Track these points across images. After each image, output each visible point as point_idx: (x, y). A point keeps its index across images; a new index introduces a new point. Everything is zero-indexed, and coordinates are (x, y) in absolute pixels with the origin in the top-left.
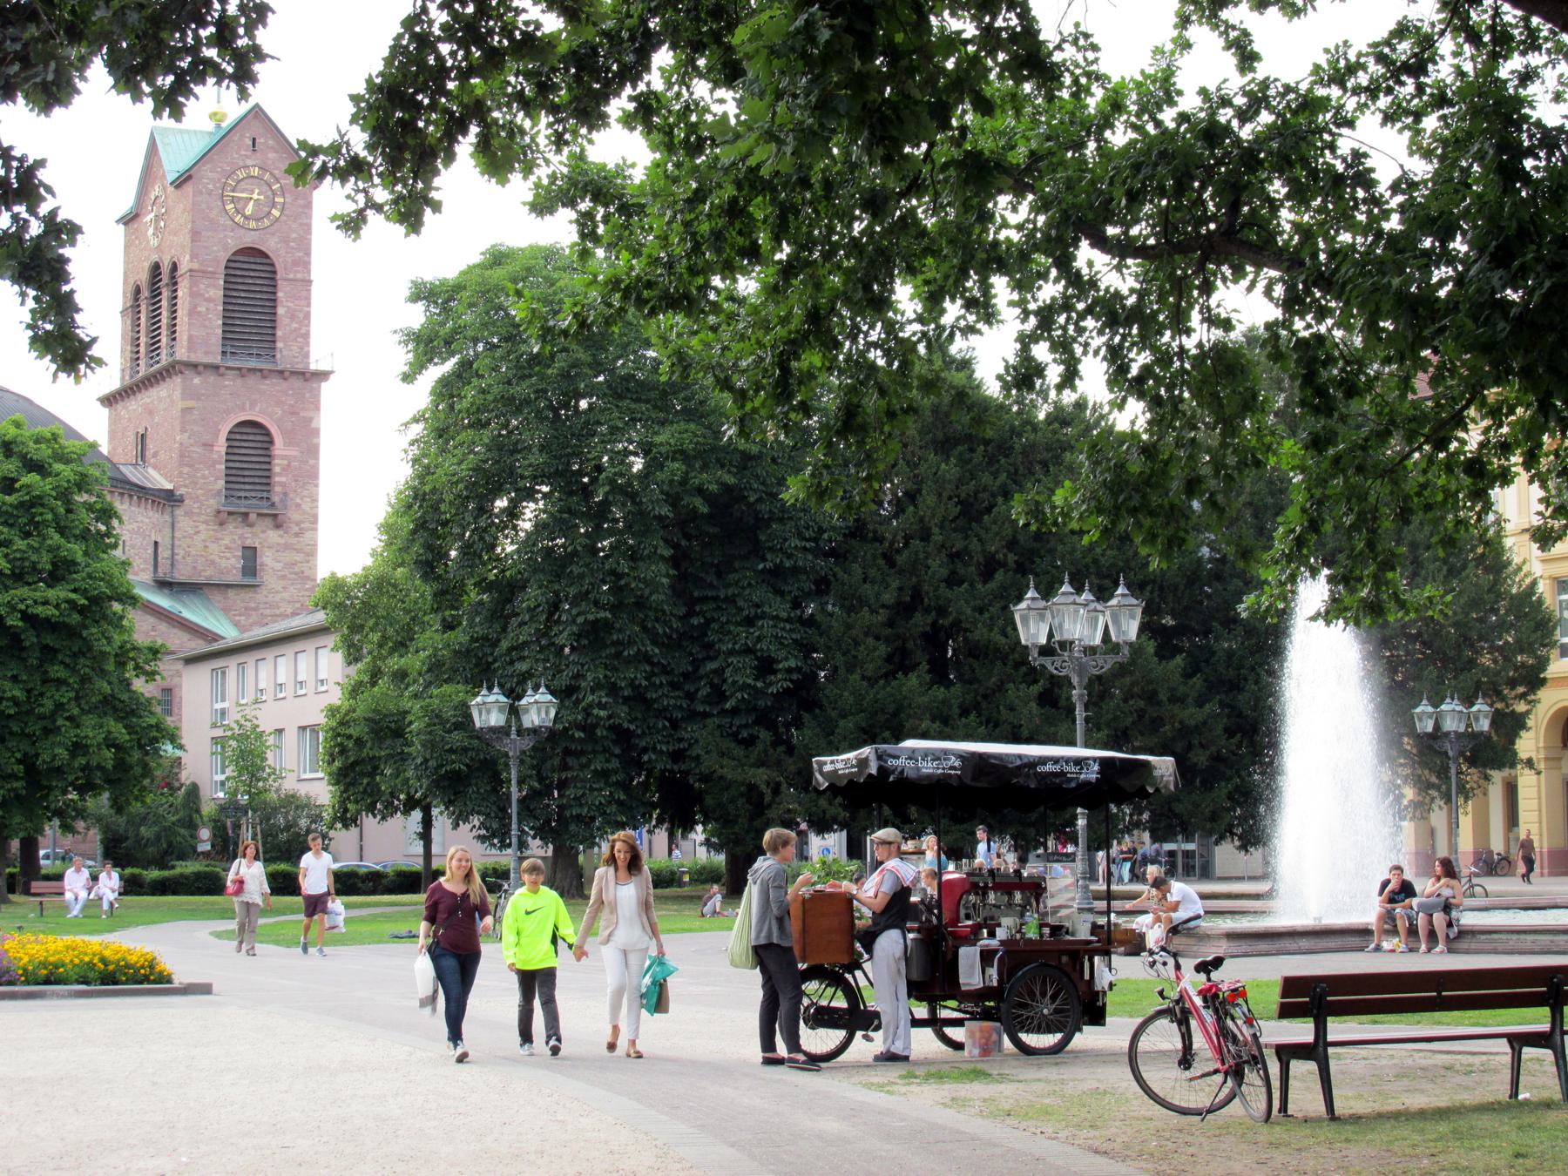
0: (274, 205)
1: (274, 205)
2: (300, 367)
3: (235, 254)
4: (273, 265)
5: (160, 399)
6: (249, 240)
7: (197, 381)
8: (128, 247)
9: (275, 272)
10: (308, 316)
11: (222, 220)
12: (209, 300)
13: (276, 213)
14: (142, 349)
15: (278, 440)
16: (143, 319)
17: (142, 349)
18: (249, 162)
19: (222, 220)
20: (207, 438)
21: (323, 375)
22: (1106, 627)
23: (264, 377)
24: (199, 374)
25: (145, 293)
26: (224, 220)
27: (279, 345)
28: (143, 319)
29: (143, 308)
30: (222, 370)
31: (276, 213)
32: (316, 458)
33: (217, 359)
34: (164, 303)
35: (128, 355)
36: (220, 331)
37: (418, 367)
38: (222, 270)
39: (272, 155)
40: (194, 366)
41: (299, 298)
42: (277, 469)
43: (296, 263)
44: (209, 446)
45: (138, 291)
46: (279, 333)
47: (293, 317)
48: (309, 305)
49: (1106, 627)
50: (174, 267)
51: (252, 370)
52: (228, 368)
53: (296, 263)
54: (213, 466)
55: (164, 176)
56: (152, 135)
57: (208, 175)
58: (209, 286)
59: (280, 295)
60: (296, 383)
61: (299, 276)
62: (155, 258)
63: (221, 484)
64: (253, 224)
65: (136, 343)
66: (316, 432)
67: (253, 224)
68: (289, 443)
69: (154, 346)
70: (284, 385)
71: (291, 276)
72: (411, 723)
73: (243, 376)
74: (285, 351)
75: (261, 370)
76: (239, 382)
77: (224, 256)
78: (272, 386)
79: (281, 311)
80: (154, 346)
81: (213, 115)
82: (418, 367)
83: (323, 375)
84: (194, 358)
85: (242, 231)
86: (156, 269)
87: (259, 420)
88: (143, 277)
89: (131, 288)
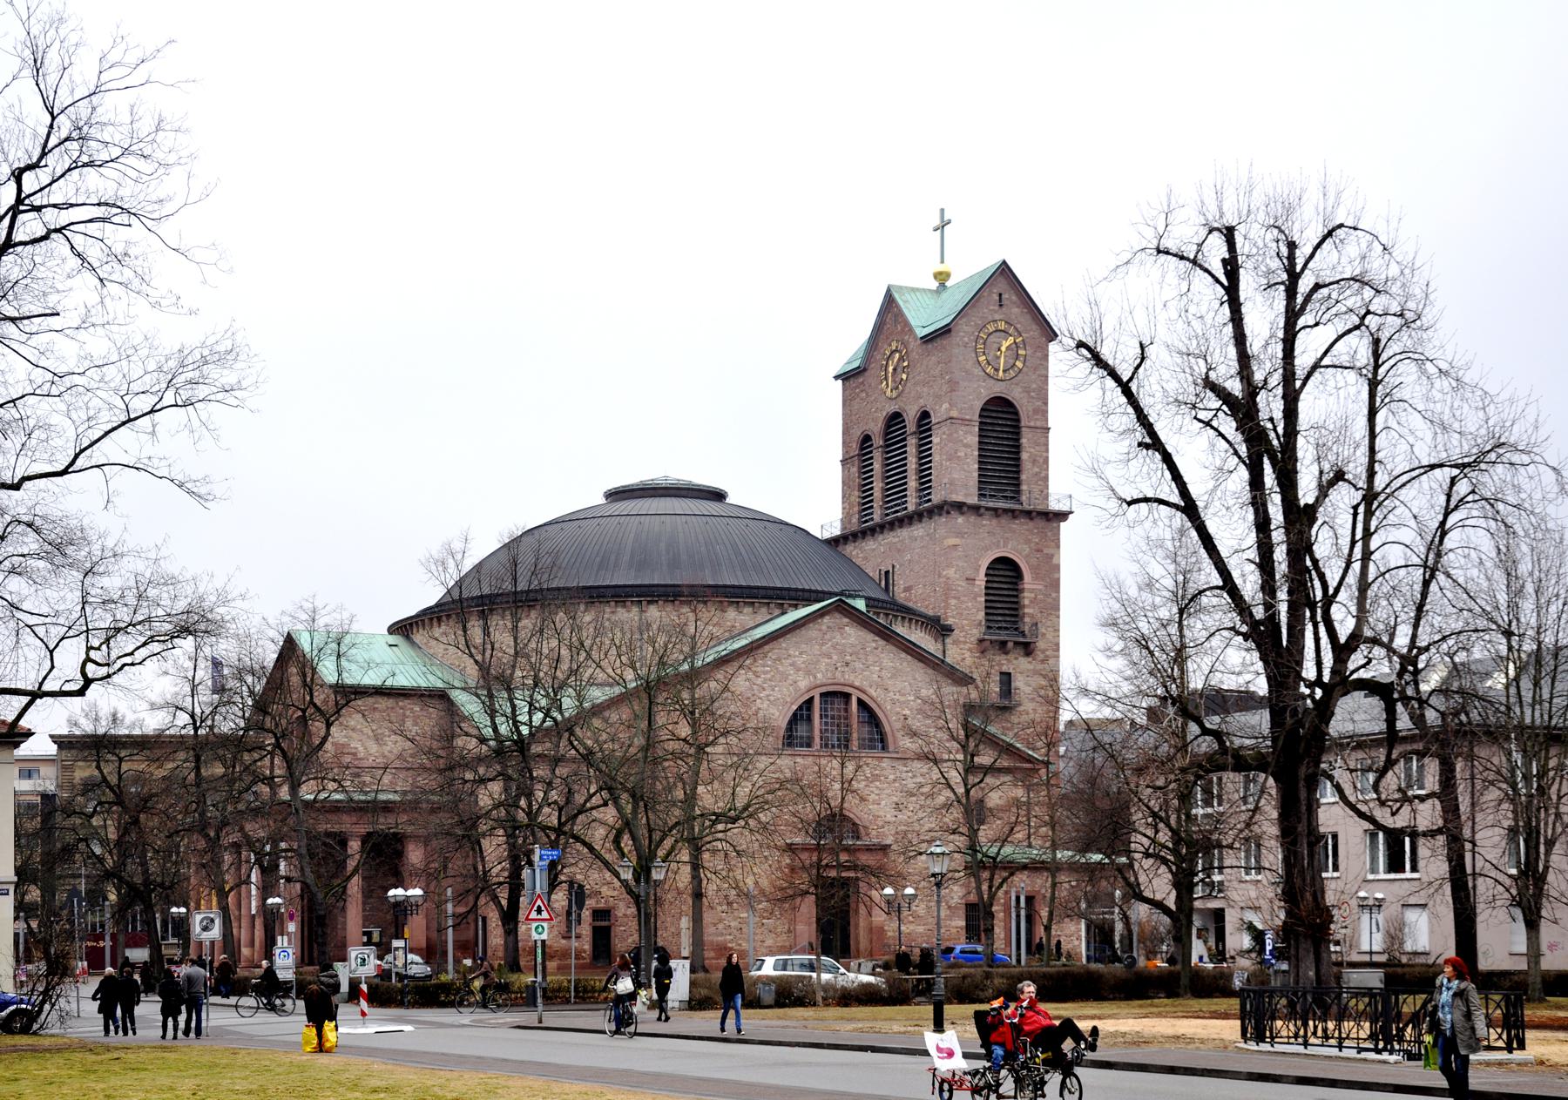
0: (1017, 357)
1: (1017, 357)
2: (1040, 508)
6: (998, 389)
7: (960, 520)
8: (847, 402)
9: (1018, 420)
12: (966, 446)
13: (1019, 364)
17: (877, 493)
18: (997, 317)
20: (969, 573)
21: (1063, 516)
23: (1015, 517)
24: (962, 513)
25: (878, 441)
26: (977, 371)
27: (1024, 487)
31: (1019, 364)
32: (1058, 591)
36: (976, 474)
38: (976, 417)
39: (1016, 310)
40: (960, 507)
41: (1038, 445)
42: (1026, 602)
43: (1036, 411)
44: (971, 580)
45: (867, 438)
46: (1023, 477)
48: (1047, 451)
50: (925, 415)
51: (1005, 511)
54: (975, 598)
57: (964, 332)
58: (966, 433)
60: (1041, 523)
61: (1039, 424)
63: (981, 615)
66: (1057, 568)
68: (1036, 577)
70: (1031, 524)
71: (1032, 424)
73: (997, 516)
74: (1027, 501)
76: (994, 522)
77: (979, 405)
78: (1021, 526)
79: (1024, 456)
80: (895, 490)
81: (937, 275)
83: (1063, 516)
85: (993, 381)
86: (895, 419)
88: (876, 428)
89: (857, 434)
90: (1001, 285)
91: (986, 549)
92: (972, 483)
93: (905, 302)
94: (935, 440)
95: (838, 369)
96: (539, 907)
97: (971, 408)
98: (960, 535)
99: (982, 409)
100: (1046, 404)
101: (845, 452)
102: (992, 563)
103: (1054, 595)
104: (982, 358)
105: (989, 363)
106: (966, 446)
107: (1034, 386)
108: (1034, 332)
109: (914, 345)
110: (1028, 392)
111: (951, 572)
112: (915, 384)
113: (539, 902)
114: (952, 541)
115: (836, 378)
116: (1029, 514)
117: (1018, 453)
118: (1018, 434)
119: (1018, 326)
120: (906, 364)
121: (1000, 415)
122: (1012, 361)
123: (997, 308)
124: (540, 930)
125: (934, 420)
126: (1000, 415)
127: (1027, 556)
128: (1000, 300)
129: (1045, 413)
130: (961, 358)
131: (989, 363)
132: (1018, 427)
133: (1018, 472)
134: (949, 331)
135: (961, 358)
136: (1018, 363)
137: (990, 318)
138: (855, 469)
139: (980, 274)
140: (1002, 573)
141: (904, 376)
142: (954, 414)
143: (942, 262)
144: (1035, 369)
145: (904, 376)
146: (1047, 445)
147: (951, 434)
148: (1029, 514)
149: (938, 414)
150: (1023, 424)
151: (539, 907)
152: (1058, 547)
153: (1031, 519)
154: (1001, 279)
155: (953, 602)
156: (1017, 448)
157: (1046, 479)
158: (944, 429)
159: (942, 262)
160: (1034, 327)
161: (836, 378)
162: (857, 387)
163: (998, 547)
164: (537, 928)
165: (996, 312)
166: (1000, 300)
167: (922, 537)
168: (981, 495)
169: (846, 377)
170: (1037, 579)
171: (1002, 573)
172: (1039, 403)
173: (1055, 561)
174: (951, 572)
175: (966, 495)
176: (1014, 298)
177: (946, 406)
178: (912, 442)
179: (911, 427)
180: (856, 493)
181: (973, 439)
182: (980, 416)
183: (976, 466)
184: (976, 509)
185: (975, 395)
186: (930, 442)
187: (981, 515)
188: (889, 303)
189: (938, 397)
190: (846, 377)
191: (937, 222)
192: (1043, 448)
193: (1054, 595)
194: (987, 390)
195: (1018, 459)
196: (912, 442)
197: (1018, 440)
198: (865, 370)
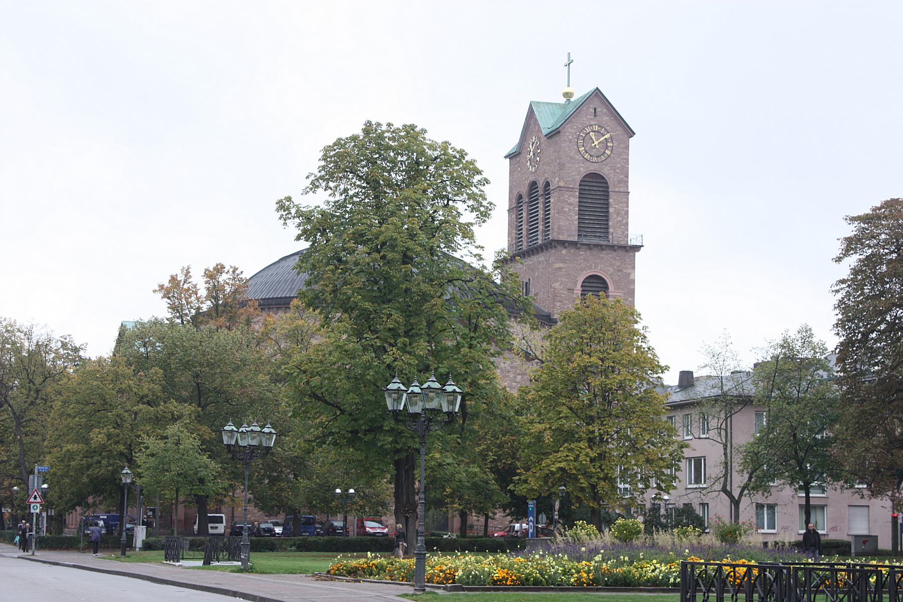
0: (607, 148)
1: (607, 148)
2: (623, 243)
3: (584, 177)
4: (607, 183)
5: (539, 263)
6: (593, 168)
7: (564, 252)
8: (512, 172)
9: (608, 187)
10: (627, 213)
11: (577, 157)
12: (570, 204)
13: (608, 152)
14: (524, 232)
15: (611, 287)
16: (524, 215)
17: (524, 232)
18: (592, 123)
19: (577, 157)
20: (570, 286)
21: (637, 248)
22: (237, 440)
23: (603, 250)
24: (565, 248)
25: (525, 199)
26: (578, 157)
27: (611, 230)
28: (524, 215)
29: (524, 207)
30: (579, 246)
31: (608, 152)
32: (633, 297)
33: (576, 239)
34: (541, 205)
35: (514, 235)
36: (577, 222)
37: (847, 252)
38: (577, 186)
39: (606, 118)
40: (563, 243)
41: (622, 203)
43: (620, 182)
44: (571, 290)
45: (520, 197)
46: (610, 223)
47: (618, 214)
48: (628, 206)
49: (237, 440)
50: (547, 184)
51: (596, 246)
52: (582, 244)
53: (620, 182)
54: (574, 302)
55: (539, 131)
56: (531, 105)
57: (569, 132)
58: (570, 196)
59: (611, 200)
60: (621, 253)
61: (621, 189)
62: (532, 178)
64: (595, 159)
65: (519, 228)
66: (633, 281)
67: (595, 159)
68: (617, 288)
69: (532, 230)
70: (614, 254)
71: (617, 190)
72: (316, 484)
73: (590, 249)
74: (614, 236)
75: (601, 246)
76: (588, 252)
77: (579, 178)
78: (606, 255)
79: (611, 210)
80: (532, 230)
82: (847, 252)
83: (637, 248)
84: (561, 238)
85: (590, 163)
86: (534, 184)
87: (600, 274)
88: (524, 190)
89: (516, 193)
90: (596, 103)
91: (582, 270)
92: (573, 228)
93: (539, 112)
94: (552, 200)
95: (506, 153)
96: (35, 496)
97: (574, 180)
98: (563, 261)
99: (581, 181)
100: (627, 177)
101: (510, 205)
102: (587, 278)
103: (630, 299)
104: (582, 149)
105: (586, 152)
106: (570, 204)
107: (619, 166)
108: (620, 131)
109: (543, 139)
110: (615, 170)
111: (557, 285)
112: (543, 164)
113: (36, 493)
114: (557, 265)
115: (506, 157)
116: (612, 247)
117: (608, 208)
118: (608, 196)
119: (608, 128)
120: (539, 151)
121: (595, 184)
122: (603, 150)
123: (592, 117)
124: (35, 507)
125: (551, 188)
126: (595, 184)
127: (611, 274)
128: (595, 113)
129: (626, 183)
130: (567, 149)
131: (586, 152)
132: (608, 192)
133: (608, 220)
134: (559, 132)
135: (567, 149)
136: (607, 151)
137: (588, 124)
138: (514, 216)
139: (590, 92)
140: (594, 285)
141: (538, 159)
142: (562, 184)
143: (569, 86)
144: (620, 155)
145: (538, 159)
146: (627, 203)
147: (559, 197)
148: (612, 247)
149: (555, 182)
150: (610, 190)
151: (35, 496)
152: (634, 268)
153: (615, 251)
154: (596, 99)
155: (558, 304)
156: (607, 205)
157: (627, 224)
158: (556, 193)
159: (569, 86)
160: (619, 128)
161: (506, 157)
162: (516, 164)
163: (591, 268)
164: (34, 506)
165: (591, 119)
166: (595, 113)
167: (543, 262)
168: (579, 235)
169: (511, 156)
170: (618, 289)
171: (594, 285)
172: (623, 176)
173: (631, 277)
174: (557, 285)
175: (569, 236)
176: (605, 110)
177: (557, 179)
178: (541, 200)
179: (541, 192)
180: (514, 231)
181: (575, 200)
182: (580, 185)
183: (577, 217)
184: (574, 244)
185: (576, 172)
186: (549, 202)
187: (578, 249)
188: (531, 114)
189: (554, 173)
190: (511, 156)
191: (566, 62)
192: (625, 205)
193: (630, 299)
194: (584, 169)
195: (608, 212)
196: (541, 200)
197: (608, 200)
198: (520, 153)
